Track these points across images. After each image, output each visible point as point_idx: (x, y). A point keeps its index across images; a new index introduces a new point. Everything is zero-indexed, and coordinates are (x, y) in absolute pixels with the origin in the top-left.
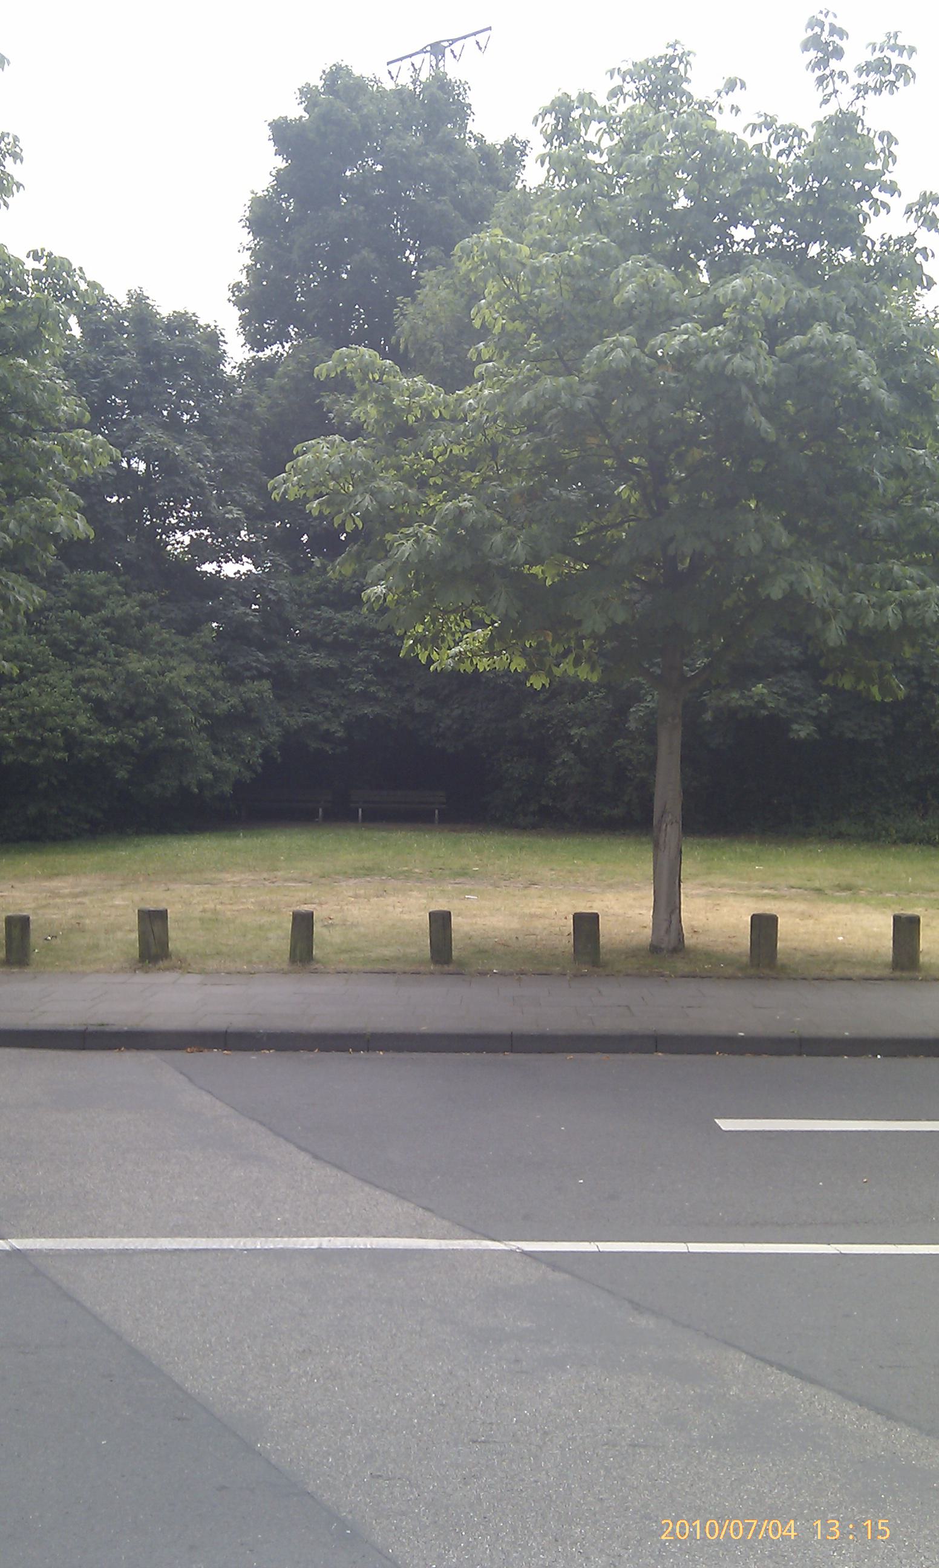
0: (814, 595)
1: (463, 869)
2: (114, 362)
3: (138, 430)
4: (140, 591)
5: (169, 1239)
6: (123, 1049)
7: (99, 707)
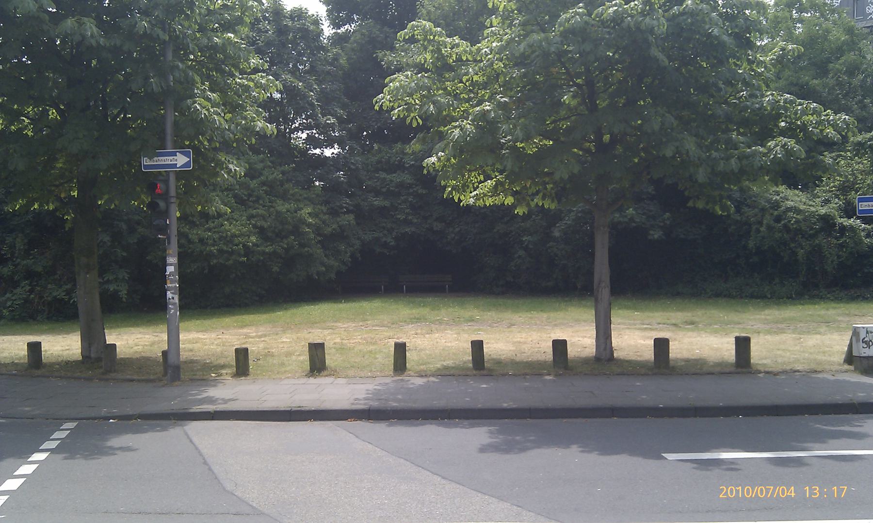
0: (691, 153)
1: (471, 318)
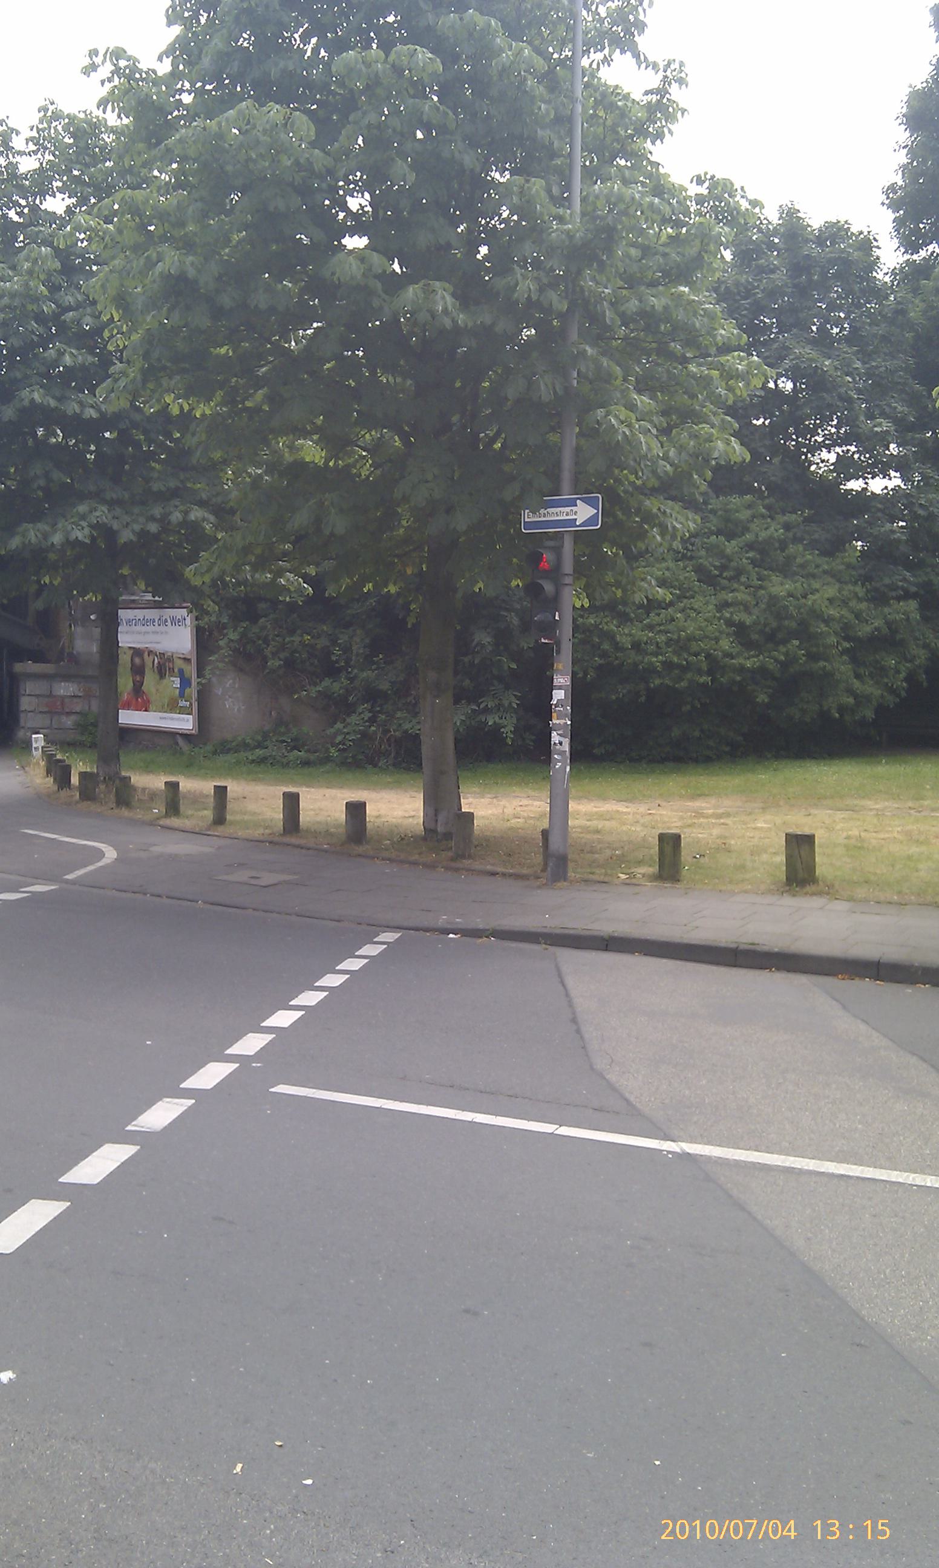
2: (764, 281)
3: (787, 348)
4: (784, 512)
5: (835, 1164)
6: (773, 969)
7: (740, 631)
